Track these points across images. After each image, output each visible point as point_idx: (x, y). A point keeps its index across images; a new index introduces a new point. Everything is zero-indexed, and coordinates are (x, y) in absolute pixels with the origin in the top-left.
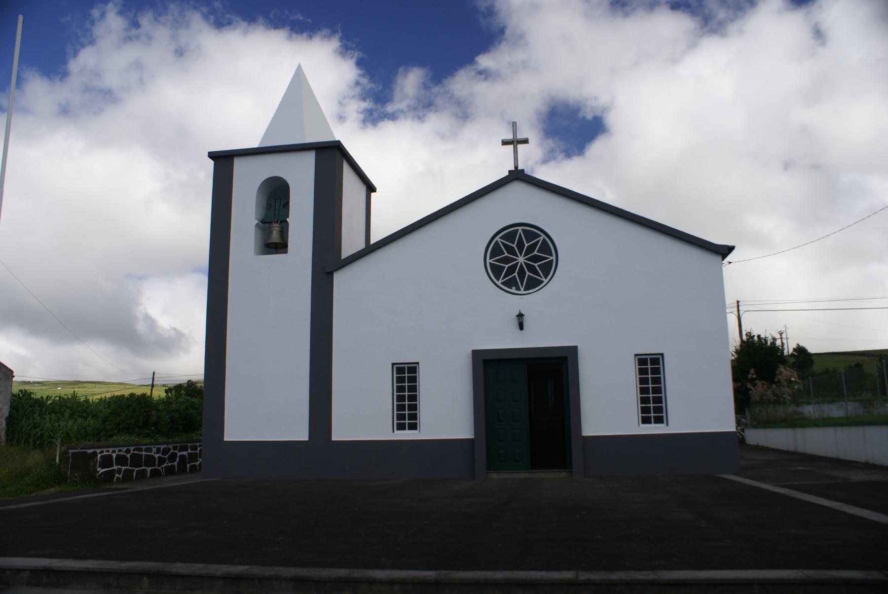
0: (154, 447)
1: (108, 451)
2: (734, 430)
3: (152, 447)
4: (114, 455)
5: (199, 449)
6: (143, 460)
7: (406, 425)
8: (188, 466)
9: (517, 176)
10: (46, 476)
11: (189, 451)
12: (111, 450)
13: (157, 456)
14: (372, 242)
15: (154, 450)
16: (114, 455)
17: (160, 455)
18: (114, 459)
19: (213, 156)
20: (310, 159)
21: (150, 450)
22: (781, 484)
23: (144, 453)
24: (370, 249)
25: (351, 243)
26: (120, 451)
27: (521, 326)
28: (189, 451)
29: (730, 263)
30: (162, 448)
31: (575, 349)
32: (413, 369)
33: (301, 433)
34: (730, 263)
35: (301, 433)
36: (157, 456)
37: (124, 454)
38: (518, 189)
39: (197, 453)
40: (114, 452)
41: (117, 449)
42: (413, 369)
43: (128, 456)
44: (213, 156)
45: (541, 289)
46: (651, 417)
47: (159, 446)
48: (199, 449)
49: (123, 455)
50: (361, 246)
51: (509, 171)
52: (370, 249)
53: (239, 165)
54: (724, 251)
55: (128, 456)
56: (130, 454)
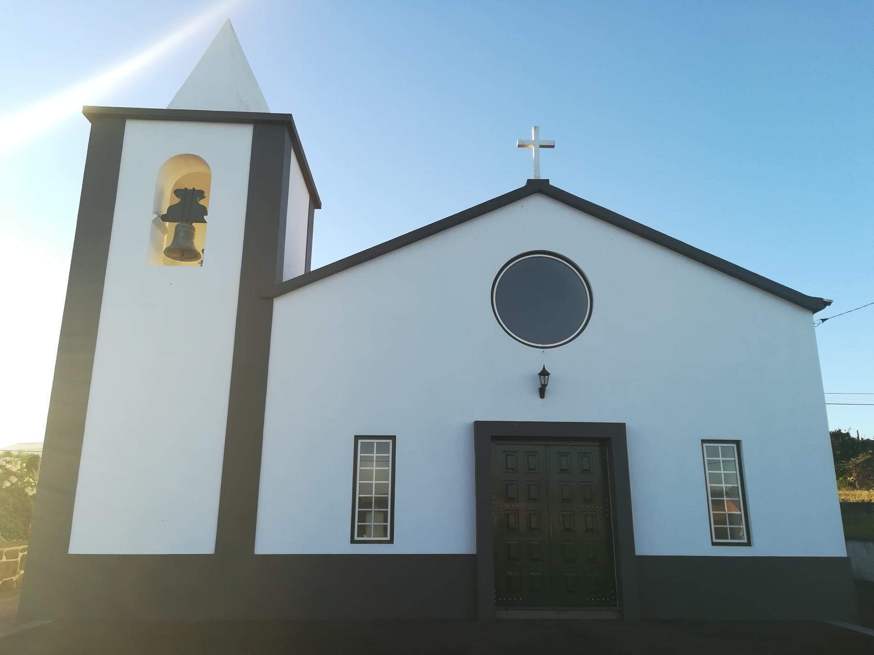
5: (21, 554)
6: (19, 566)
7: (715, 500)
14: (313, 268)
20: (244, 135)
24: (311, 277)
25: (293, 268)
27: (542, 392)
29: (823, 320)
32: (492, 437)
34: (823, 320)
38: (537, 204)
39: (17, 562)
42: (492, 437)
46: (724, 500)
50: (301, 272)
51: (194, 189)
52: (311, 277)
53: (133, 130)
54: (815, 305)
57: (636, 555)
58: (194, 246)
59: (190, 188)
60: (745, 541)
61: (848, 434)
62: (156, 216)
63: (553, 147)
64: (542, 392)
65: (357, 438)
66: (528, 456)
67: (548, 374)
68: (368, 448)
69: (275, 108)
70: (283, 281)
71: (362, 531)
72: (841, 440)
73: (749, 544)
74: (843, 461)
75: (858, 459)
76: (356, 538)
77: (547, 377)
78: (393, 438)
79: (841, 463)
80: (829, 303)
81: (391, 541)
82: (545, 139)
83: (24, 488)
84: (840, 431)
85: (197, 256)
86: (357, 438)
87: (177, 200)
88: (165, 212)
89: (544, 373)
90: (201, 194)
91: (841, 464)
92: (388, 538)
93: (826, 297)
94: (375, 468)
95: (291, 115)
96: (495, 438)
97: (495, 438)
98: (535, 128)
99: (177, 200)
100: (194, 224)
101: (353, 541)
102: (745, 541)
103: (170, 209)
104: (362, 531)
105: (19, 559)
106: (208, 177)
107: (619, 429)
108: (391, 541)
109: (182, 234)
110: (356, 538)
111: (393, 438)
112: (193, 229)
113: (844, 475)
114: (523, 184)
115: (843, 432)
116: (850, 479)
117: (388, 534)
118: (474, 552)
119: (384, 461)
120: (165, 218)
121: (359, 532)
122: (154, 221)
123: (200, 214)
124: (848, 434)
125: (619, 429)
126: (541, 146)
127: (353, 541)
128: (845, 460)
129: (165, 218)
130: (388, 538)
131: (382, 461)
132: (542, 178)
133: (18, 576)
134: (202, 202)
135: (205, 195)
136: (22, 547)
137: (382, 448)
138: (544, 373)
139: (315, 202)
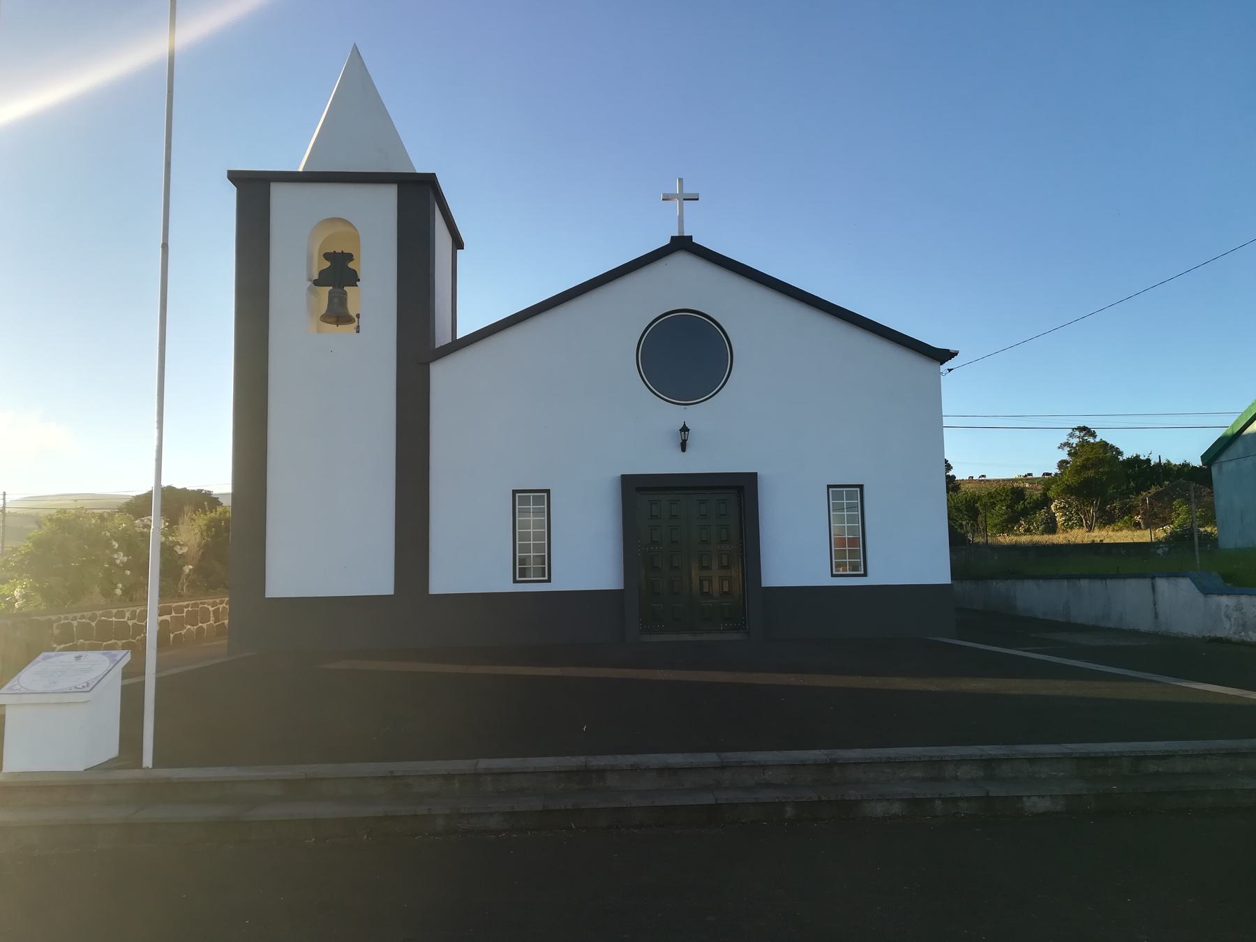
0: (128, 611)
1: (66, 618)
2: (950, 583)
3: (125, 609)
4: (75, 623)
8: (172, 636)
9: (682, 244)
10: (1023, 507)
11: (173, 614)
12: (71, 616)
13: (130, 623)
14: (460, 335)
15: (128, 614)
16: (75, 623)
17: (135, 621)
18: (171, 640)
19: (235, 177)
20: (388, 196)
21: (121, 615)
22: (1032, 648)
23: (114, 619)
26: (83, 617)
27: (683, 447)
28: (173, 614)
29: (950, 370)
30: (138, 611)
31: (753, 476)
33: (382, 582)
34: (950, 370)
35: (382, 582)
36: (130, 623)
37: (88, 621)
38: (682, 261)
40: (75, 619)
41: (78, 615)
42: (544, 494)
43: (93, 624)
44: (235, 177)
45: (718, 391)
47: (135, 609)
48: (185, 610)
49: (87, 623)
53: (279, 195)
54: (943, 356)
55: (93, 624)
56: (96, 622)
57: (763, 586)
58: (348, 311)
59: (339, 251)
60: (862, 572)
61: (1148, 461)
62: (310, 283)
63: (698, 199)
64: (683, 447)
65: (515, 492)
66: (671, 504)
67: (688, 430)
68: (525, 501)
69: (421, 168)
70: (436, 347)
71: (523, 572)
72: (1137, 469)
73: (865, 575)
74: (1131, 496)
75: (1150, 493)
76: (518, 579)
77: (687, 433)
78: (548, 491)
79: (1129, 498)
80: (953, 354)
81: (549, 581)
82: (689, 190)
83: (173, 547)
84: (1138, 456)
85: (351, 321)
86: (515, 492)
87: (327, 264)
88: (316, 277)
89: (685, 429)
90: (349, 257)
91: (1128, 500)
92: (546, 578)
93: (952, 348)
94: (532, 518)
95: (434, 174)
96: (638, 489)
97: (638, 489)
98: (680, 180)
99: (327, 264)
100: (346, 288)
101: (515, 581)
102: (862, 572)
103: (321, 273)
104: (523, 572)
105: (184, 614)
106: (356, 238)
107: (752, 478)
108: (549, 581)
109: (336, 300)
110: (518, 579)
111: (548, 491)
112: (345, 293)
113: (1130, 513)
114: (667, 241)
115: (1142, 458)
116: (1137, 518)
117: (545, 573)
118: (623, 588)
119: (540, 512)
120: (316, 283)
121: (520, 572)
122: (309, 289)
123: (353, 279)
124: (1148, 461)
125: (752, 478)
126: (684, 200)
127: (515, 581)
128: (1133, 495)
129: (316, 283)
130: (546, 578)
131: (525, 536)
132: (686, 234)
133: (185, 630)
134: (351, 265)
135: (354, 257)
136: (186, 603)
137: (538, 501)
138: (685, 429)
139: (458, 243)
